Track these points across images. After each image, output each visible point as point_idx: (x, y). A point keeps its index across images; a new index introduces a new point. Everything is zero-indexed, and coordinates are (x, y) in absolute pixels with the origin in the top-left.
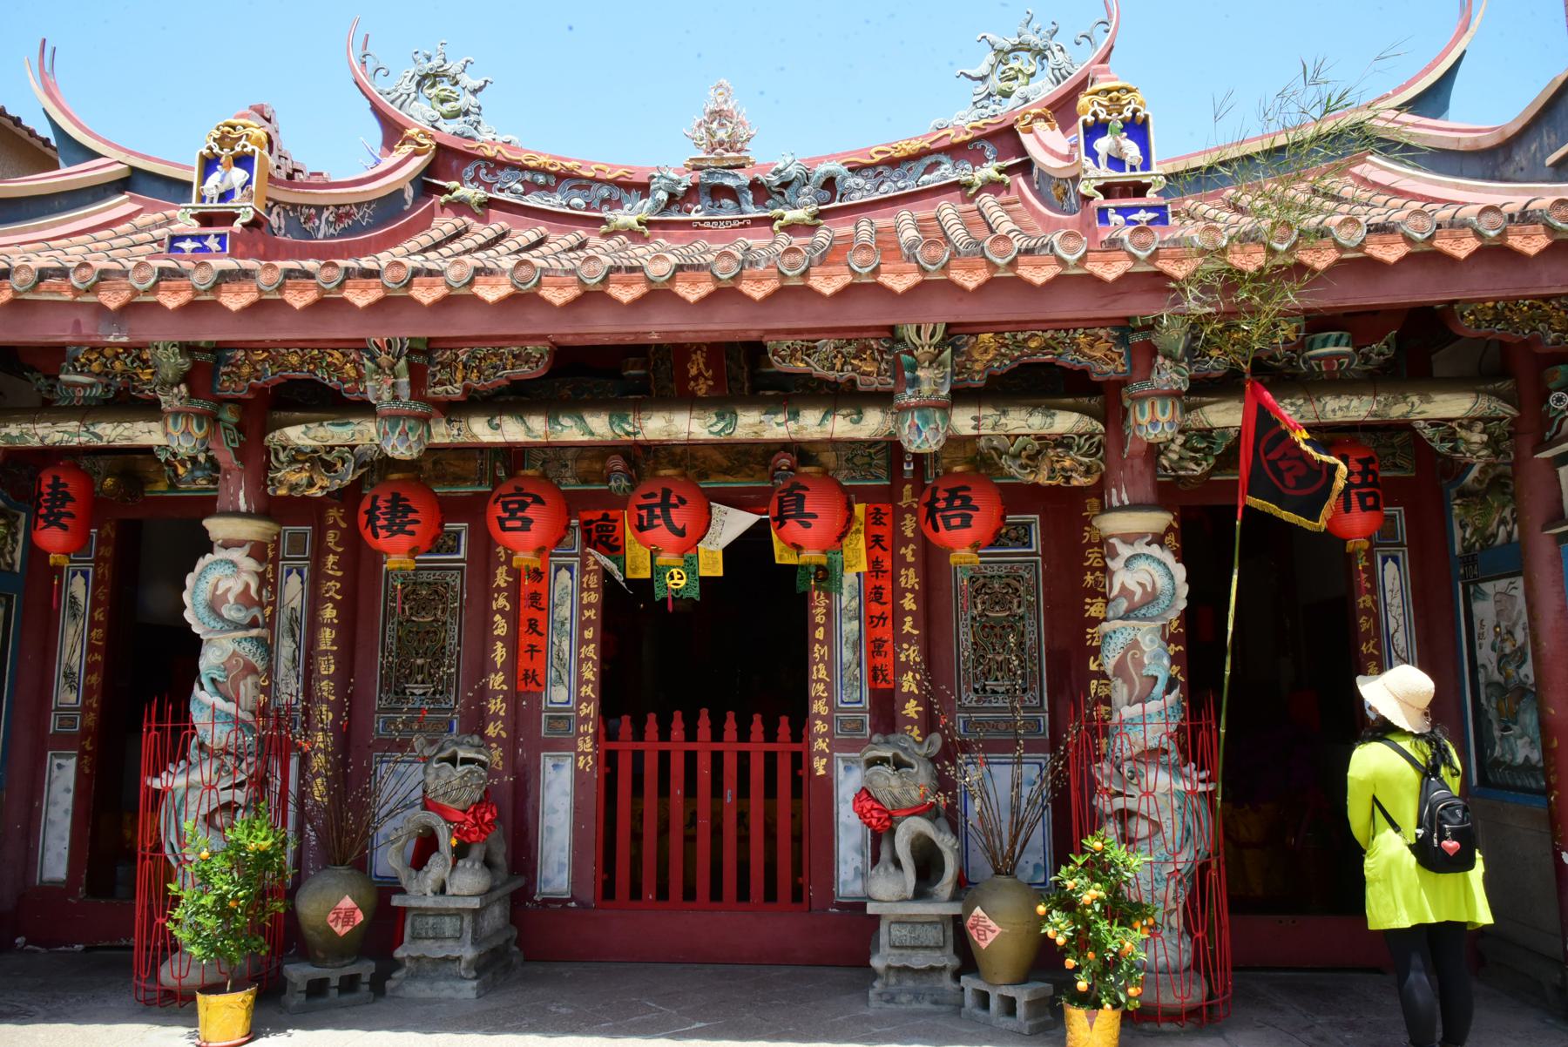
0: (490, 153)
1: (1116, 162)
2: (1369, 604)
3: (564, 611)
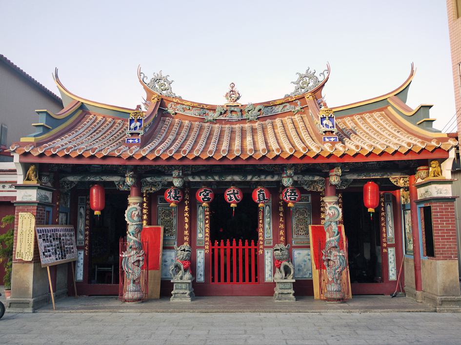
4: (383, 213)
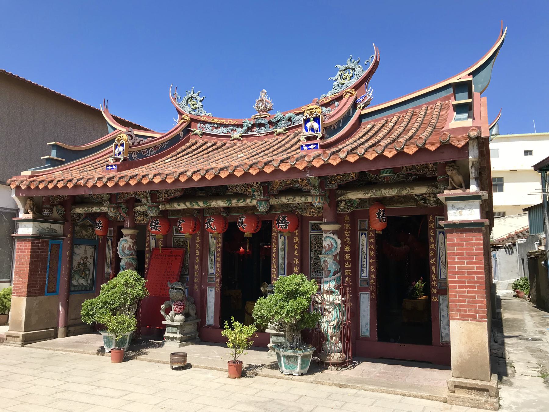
2: (433, 247)
3: (213, 249)
4: (433, 245)
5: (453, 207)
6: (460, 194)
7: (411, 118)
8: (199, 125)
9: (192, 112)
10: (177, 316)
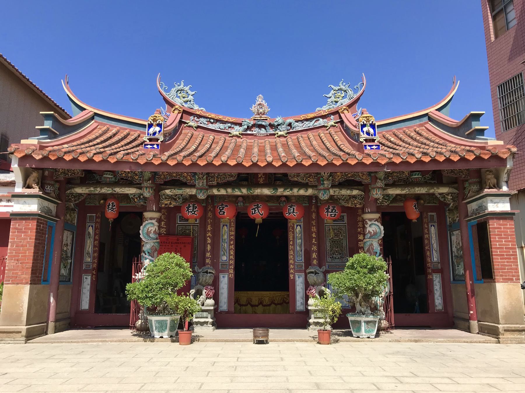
0: (198, 113)
1: (368, 133)
5: (492, 202)
6: (495, 192)
7: (190, 140)
8: (192, 118)
9: (184, 104)
10: (208, 300)
